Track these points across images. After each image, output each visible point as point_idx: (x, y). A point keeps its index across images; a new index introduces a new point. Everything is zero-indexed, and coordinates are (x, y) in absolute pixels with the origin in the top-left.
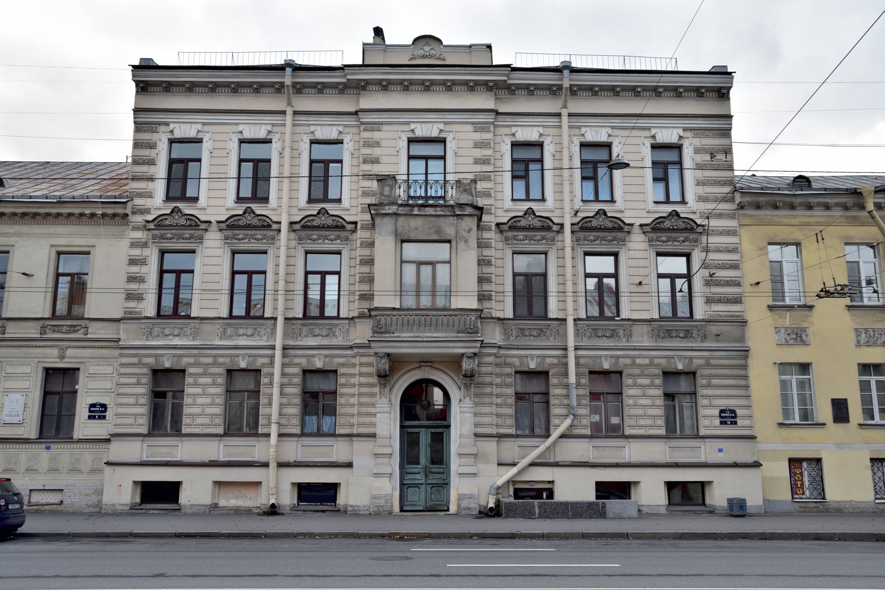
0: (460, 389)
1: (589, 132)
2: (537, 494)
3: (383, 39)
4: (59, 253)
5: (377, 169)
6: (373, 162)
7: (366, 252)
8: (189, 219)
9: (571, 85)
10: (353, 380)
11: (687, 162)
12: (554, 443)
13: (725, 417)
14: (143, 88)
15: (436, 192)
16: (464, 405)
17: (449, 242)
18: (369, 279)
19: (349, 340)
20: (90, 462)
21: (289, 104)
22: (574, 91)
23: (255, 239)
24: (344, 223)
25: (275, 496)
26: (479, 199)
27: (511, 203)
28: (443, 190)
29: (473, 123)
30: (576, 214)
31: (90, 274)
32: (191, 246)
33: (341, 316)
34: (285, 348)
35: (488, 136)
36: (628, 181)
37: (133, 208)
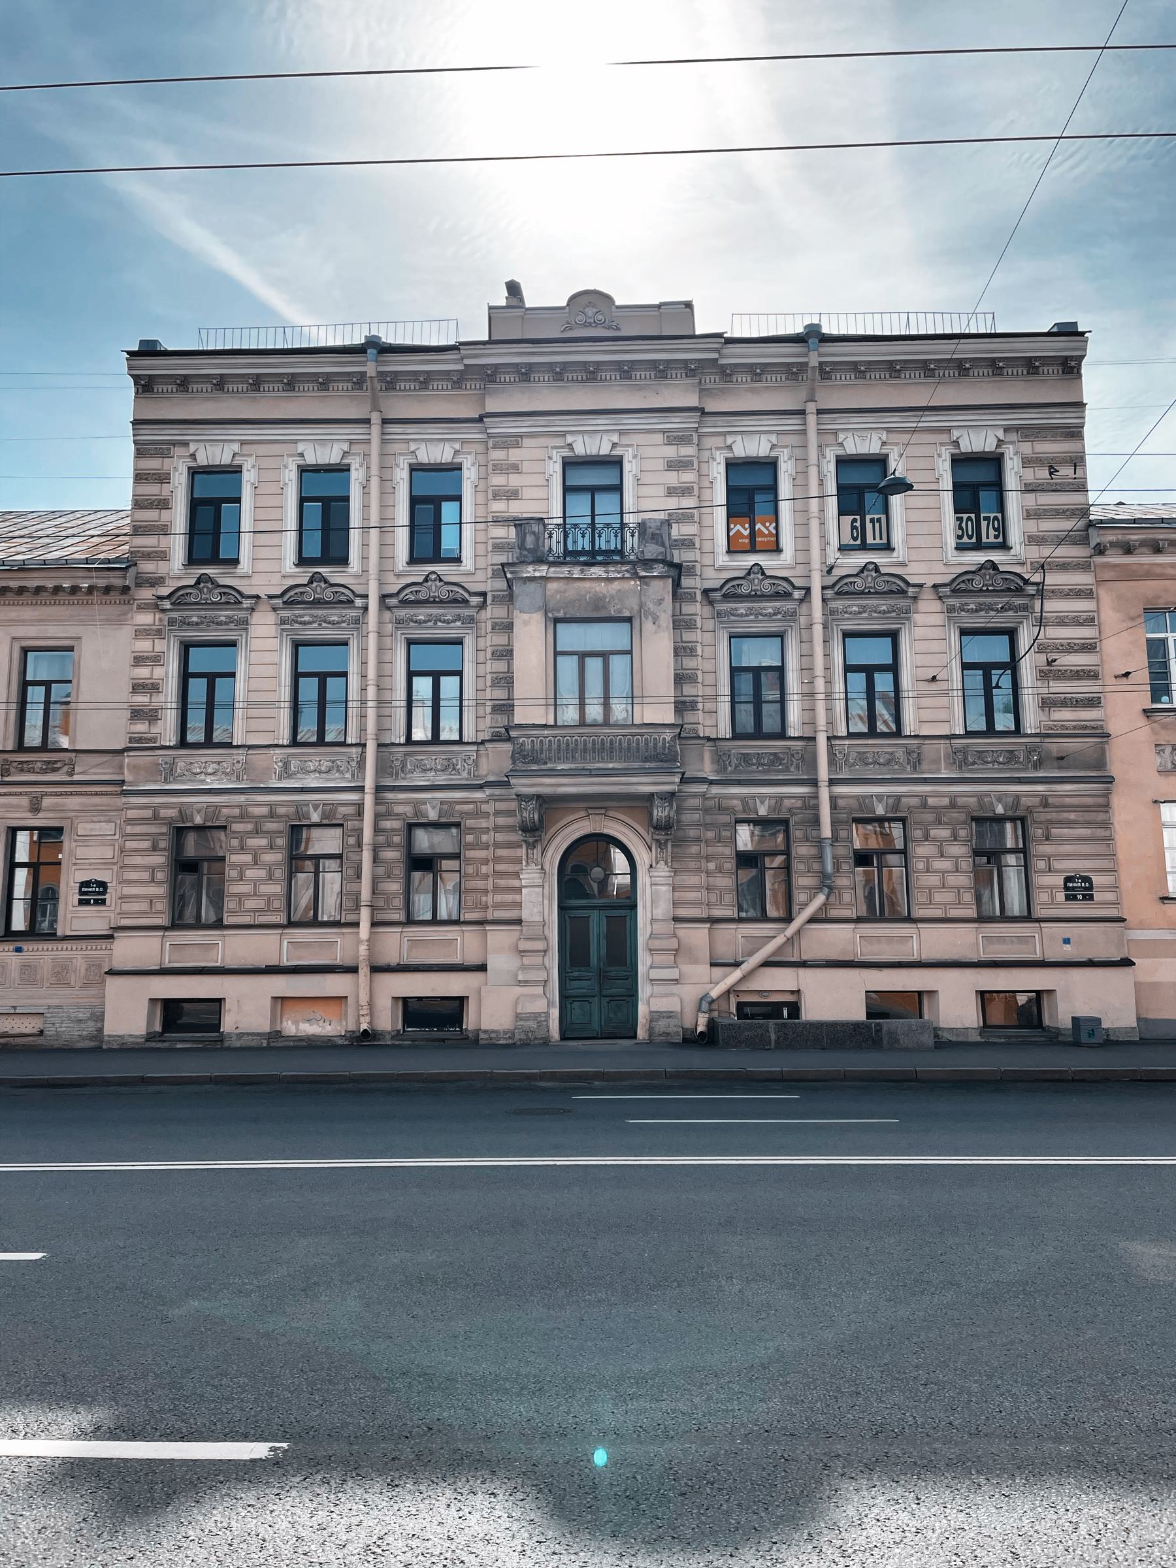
0: (650, 849)
1: (850, 439)
2: (772, 1010)
3: (522, 300)
4: (25, 651)
5: (517, 509)
6: (508, 498)
7: (501, 639)
8: (224, 593)
9: (821, 363)
10: (484, 838)
11: (1011, 481)
12: (798, 932)
13: (1074, 889)
14: (145, 386)
15: (608, 542)
16: (656, 874)
17: (629, 620)
18: (506, 680)
19: (478, 776)
20: (83, 971)
21: (375, 408)
22: (826, 371)
23: (330, 623)
24: (466, 595)
25: (368, 1019)
26: (676, 553)
27: (726, 558)
28: (619, 538)
29: (663, 431)
30: (829, 571)
31: (75, 682)
32: (230, 636)
33: (465, 740)
34: (379, 789)
35: (688, 451)
36: (915, 515)
37: (137, 578)
